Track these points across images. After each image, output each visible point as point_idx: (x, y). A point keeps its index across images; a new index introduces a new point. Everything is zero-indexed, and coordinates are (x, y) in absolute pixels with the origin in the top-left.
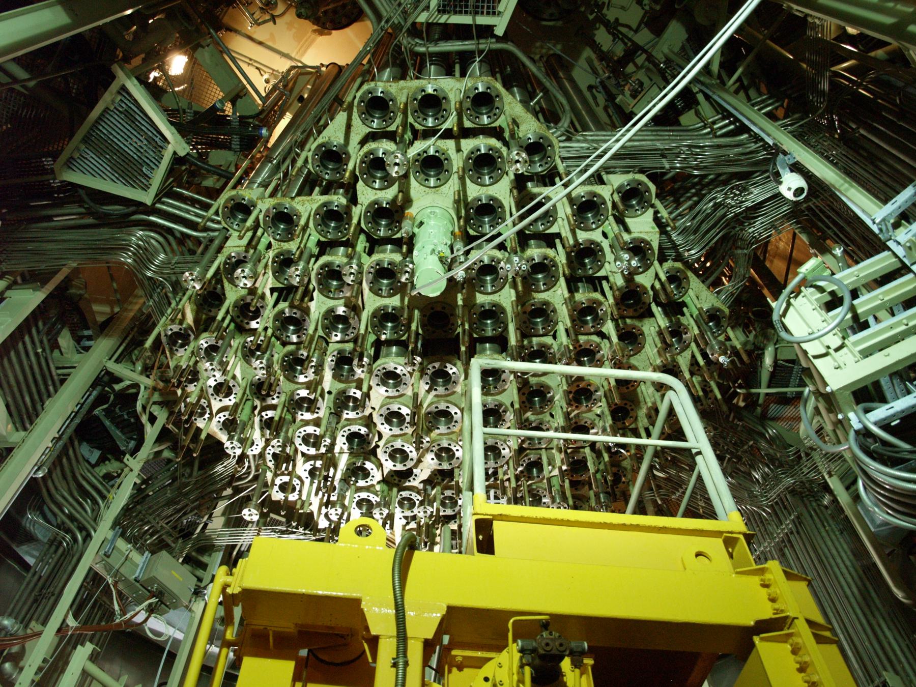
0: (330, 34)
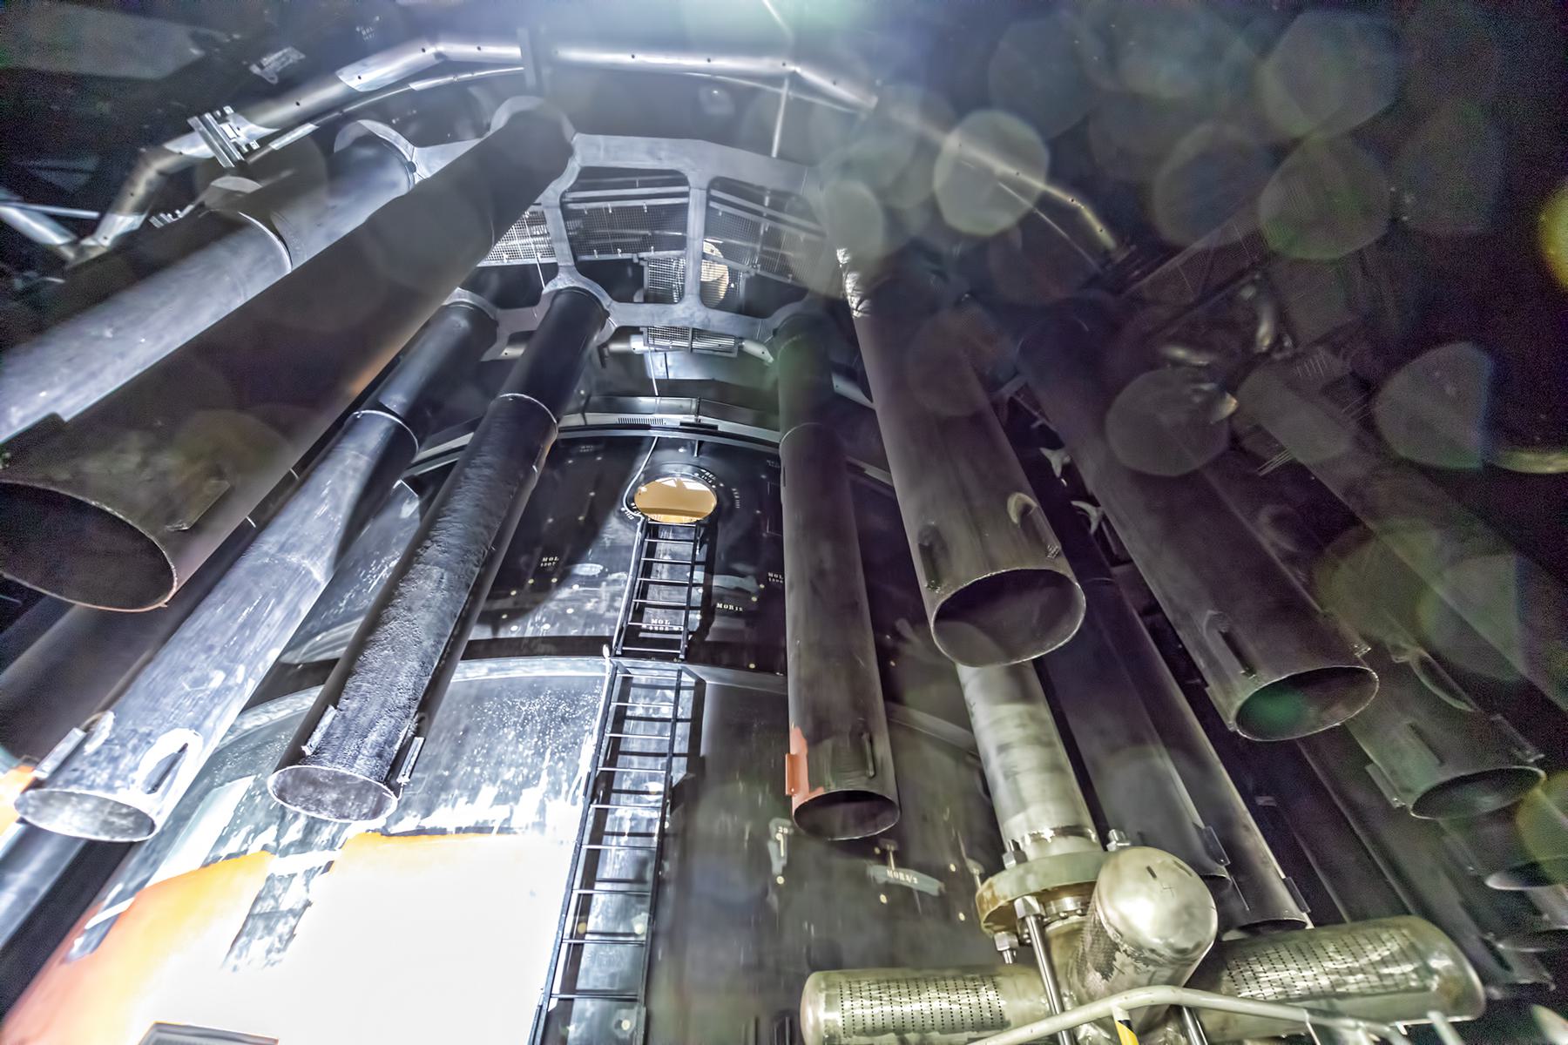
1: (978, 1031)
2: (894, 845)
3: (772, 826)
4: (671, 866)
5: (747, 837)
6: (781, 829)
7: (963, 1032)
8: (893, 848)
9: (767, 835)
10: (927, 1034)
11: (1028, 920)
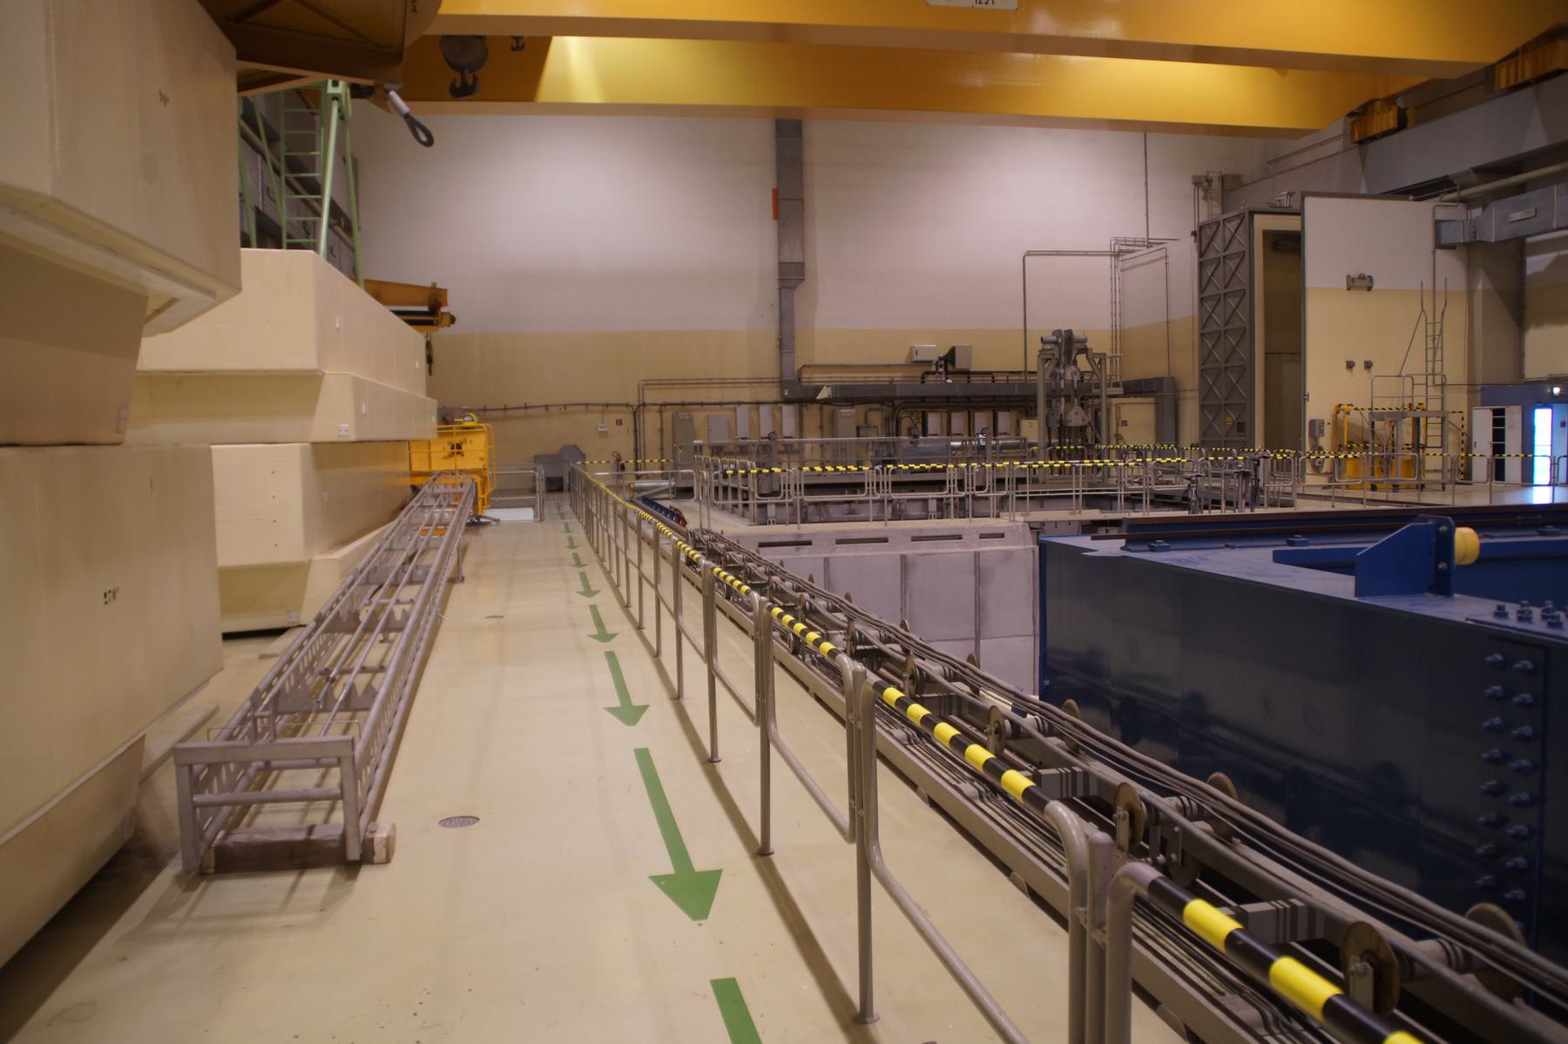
0: (705, 662)
4: (1177, 856)
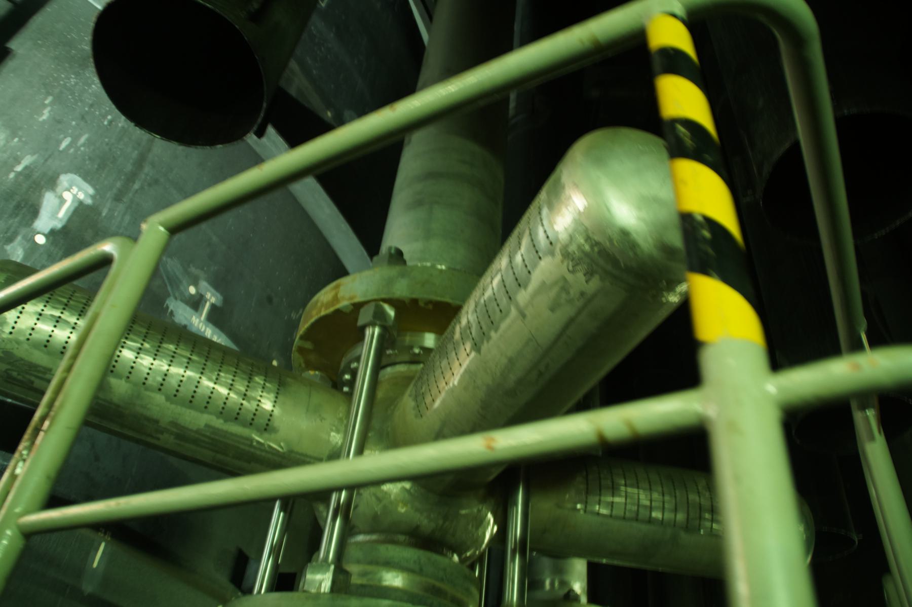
1: (226, 421)
2: (217, 298)
3: (65, 179)
5: (19, 168)
6: (75, 190)
7: (202, 412)
8: (213, 300)
9: (51, 182)
10: (148, 393)
11: (368, 332)
